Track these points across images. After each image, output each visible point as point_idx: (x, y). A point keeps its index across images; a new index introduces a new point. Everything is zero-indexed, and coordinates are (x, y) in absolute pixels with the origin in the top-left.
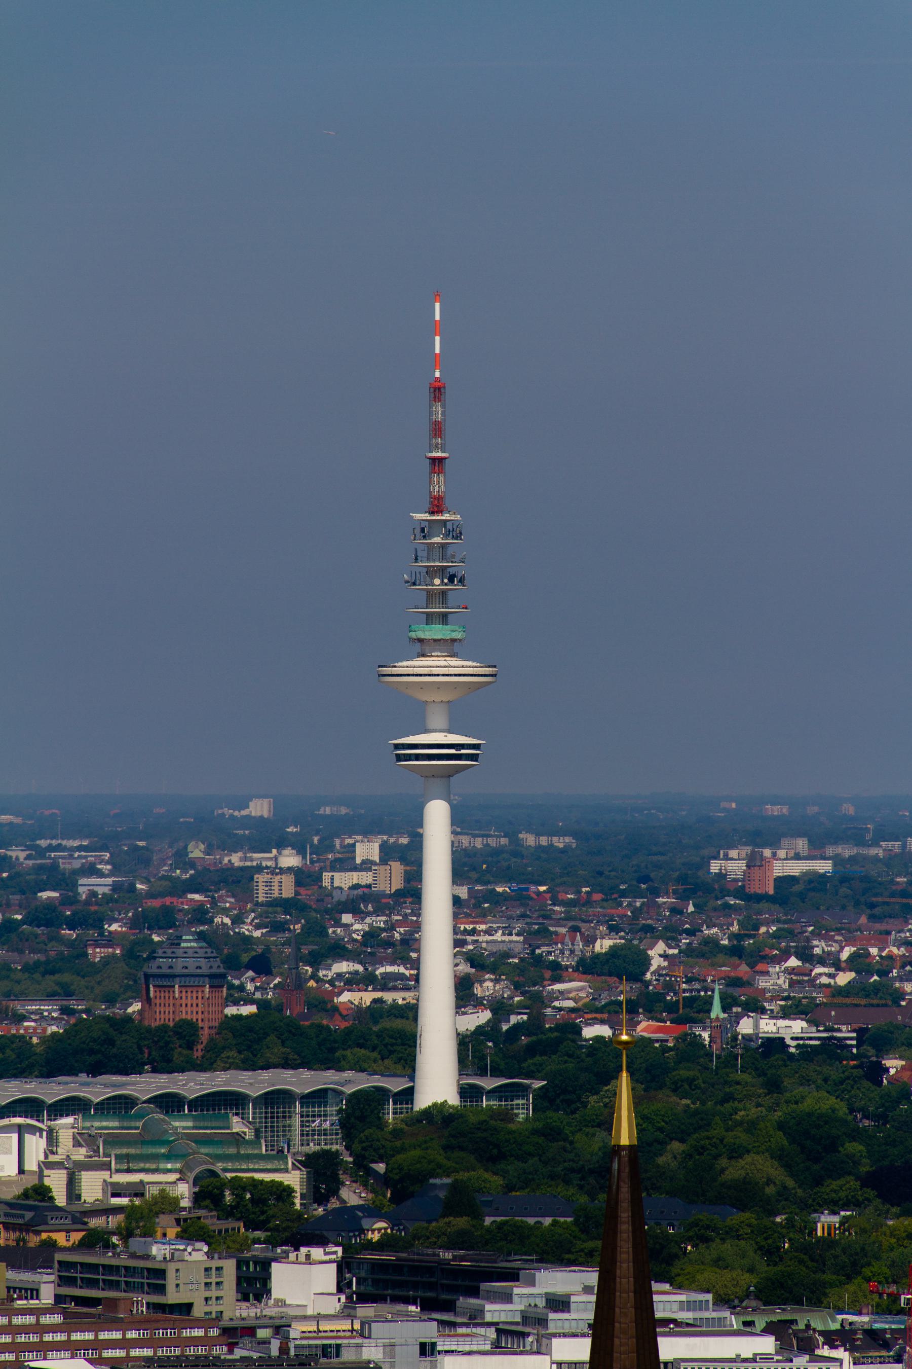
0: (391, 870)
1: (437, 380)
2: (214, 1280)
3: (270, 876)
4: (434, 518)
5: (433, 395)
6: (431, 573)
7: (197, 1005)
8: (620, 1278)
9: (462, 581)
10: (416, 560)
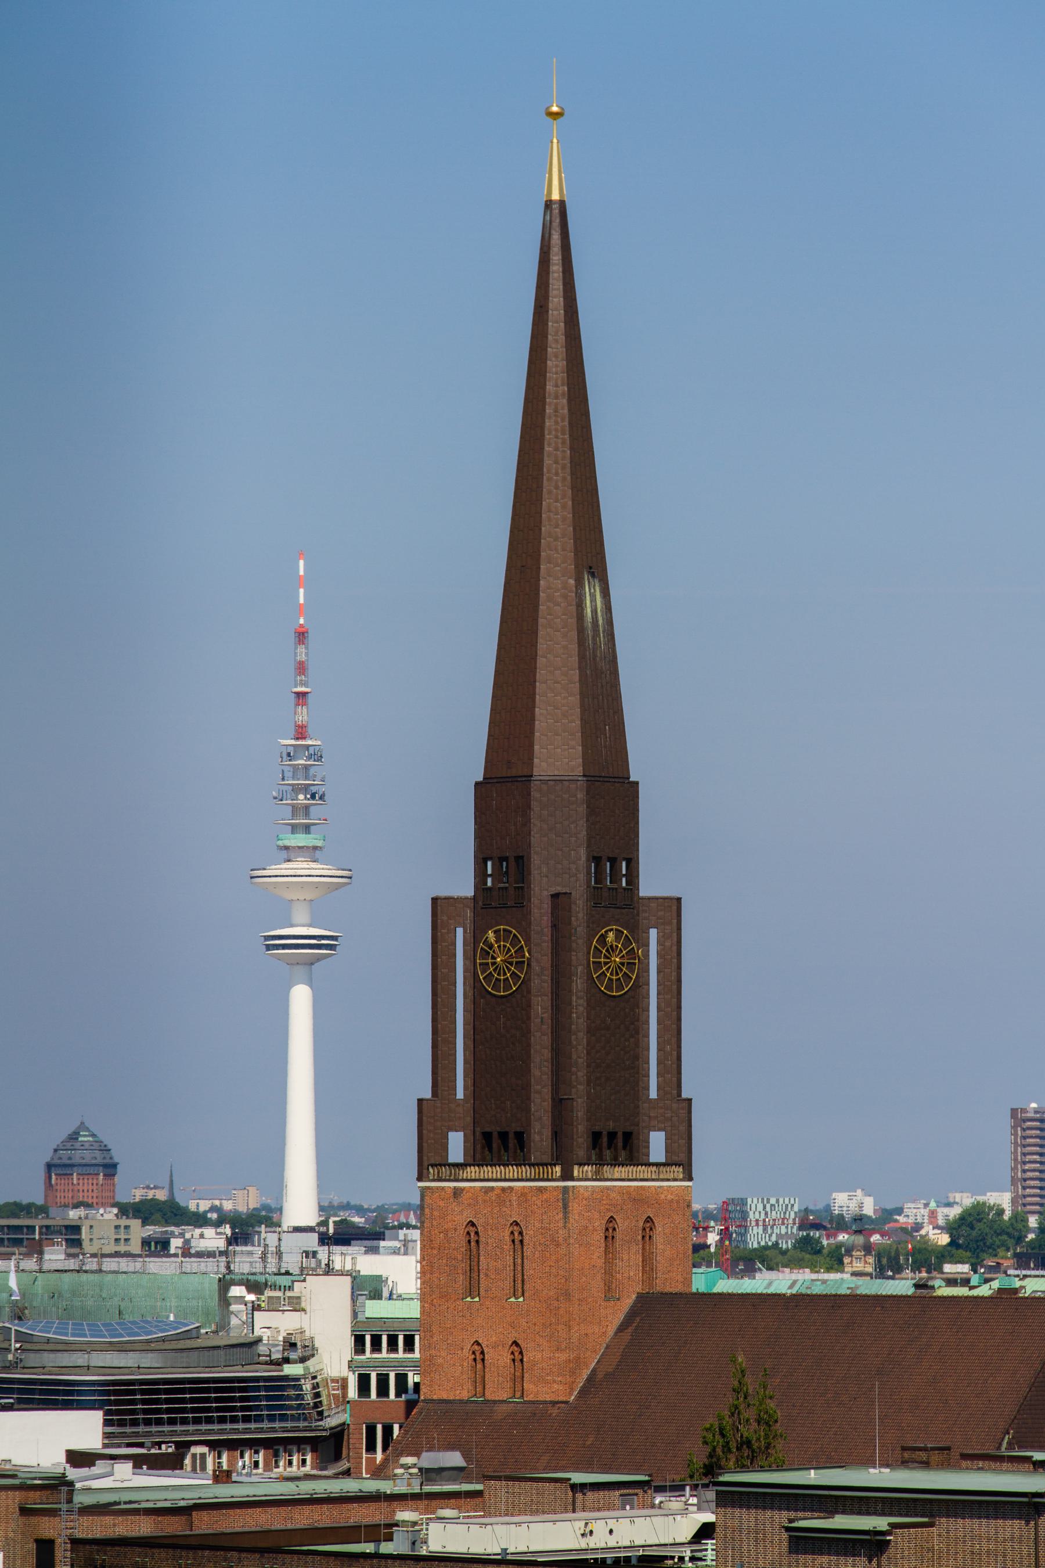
0: (248, 1194)
1: (301, 626)
2: (123, 1237)
3: (145, 1190)
4: (298, 743)
5: (297, 639)
6: (296, 789)
7: (93, 1191)
8: (552, 310)
9: (322, 798)
10: (283, 779)
